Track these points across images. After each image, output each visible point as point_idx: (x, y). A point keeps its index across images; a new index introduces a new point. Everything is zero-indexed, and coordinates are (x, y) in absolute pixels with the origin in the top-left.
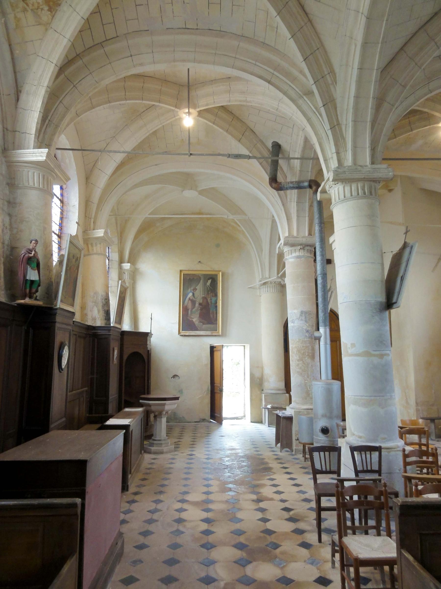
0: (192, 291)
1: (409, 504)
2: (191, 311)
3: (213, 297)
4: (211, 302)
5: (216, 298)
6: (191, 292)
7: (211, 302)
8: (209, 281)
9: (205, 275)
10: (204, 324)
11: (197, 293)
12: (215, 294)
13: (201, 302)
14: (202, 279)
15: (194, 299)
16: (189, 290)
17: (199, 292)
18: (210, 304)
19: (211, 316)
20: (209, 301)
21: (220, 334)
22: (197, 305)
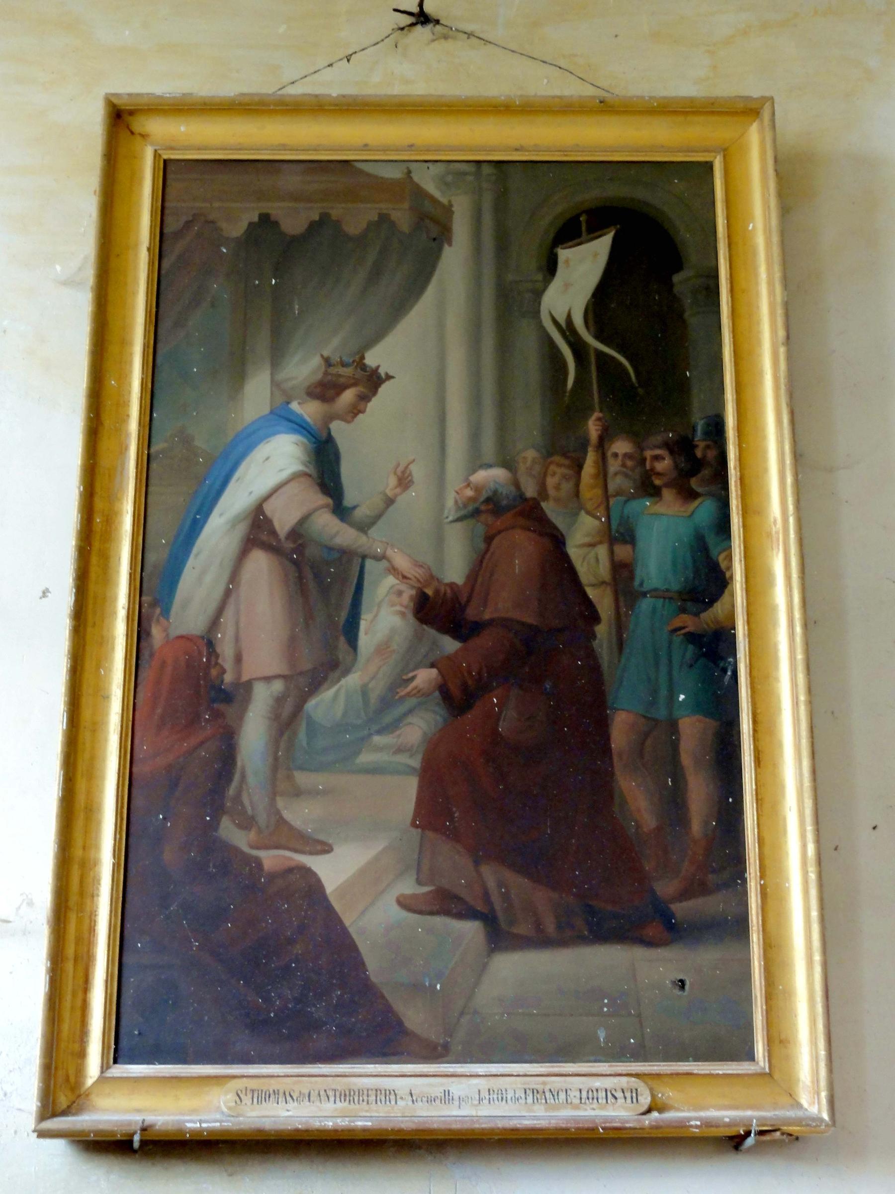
0: (308, 410)
1: (273, 1138)
2: (287, 721)
3: (649, 488)
4: (622, 575)
5: (705, 509)
6: (282, 418)
7: (622, 575)
8: (584, 265)
9: (502, 176)
10: (499, 937)
11: (380, 441)
12: (682, 447)
13: (455, 570)
14: (461, 228)
15: (327, 526)
16: (257, 394)
17: (424, 427)
18: (603, 600)
19: (637, 798)
20: (590, 561)
21: (812, 1102)
22: (385, 619)
